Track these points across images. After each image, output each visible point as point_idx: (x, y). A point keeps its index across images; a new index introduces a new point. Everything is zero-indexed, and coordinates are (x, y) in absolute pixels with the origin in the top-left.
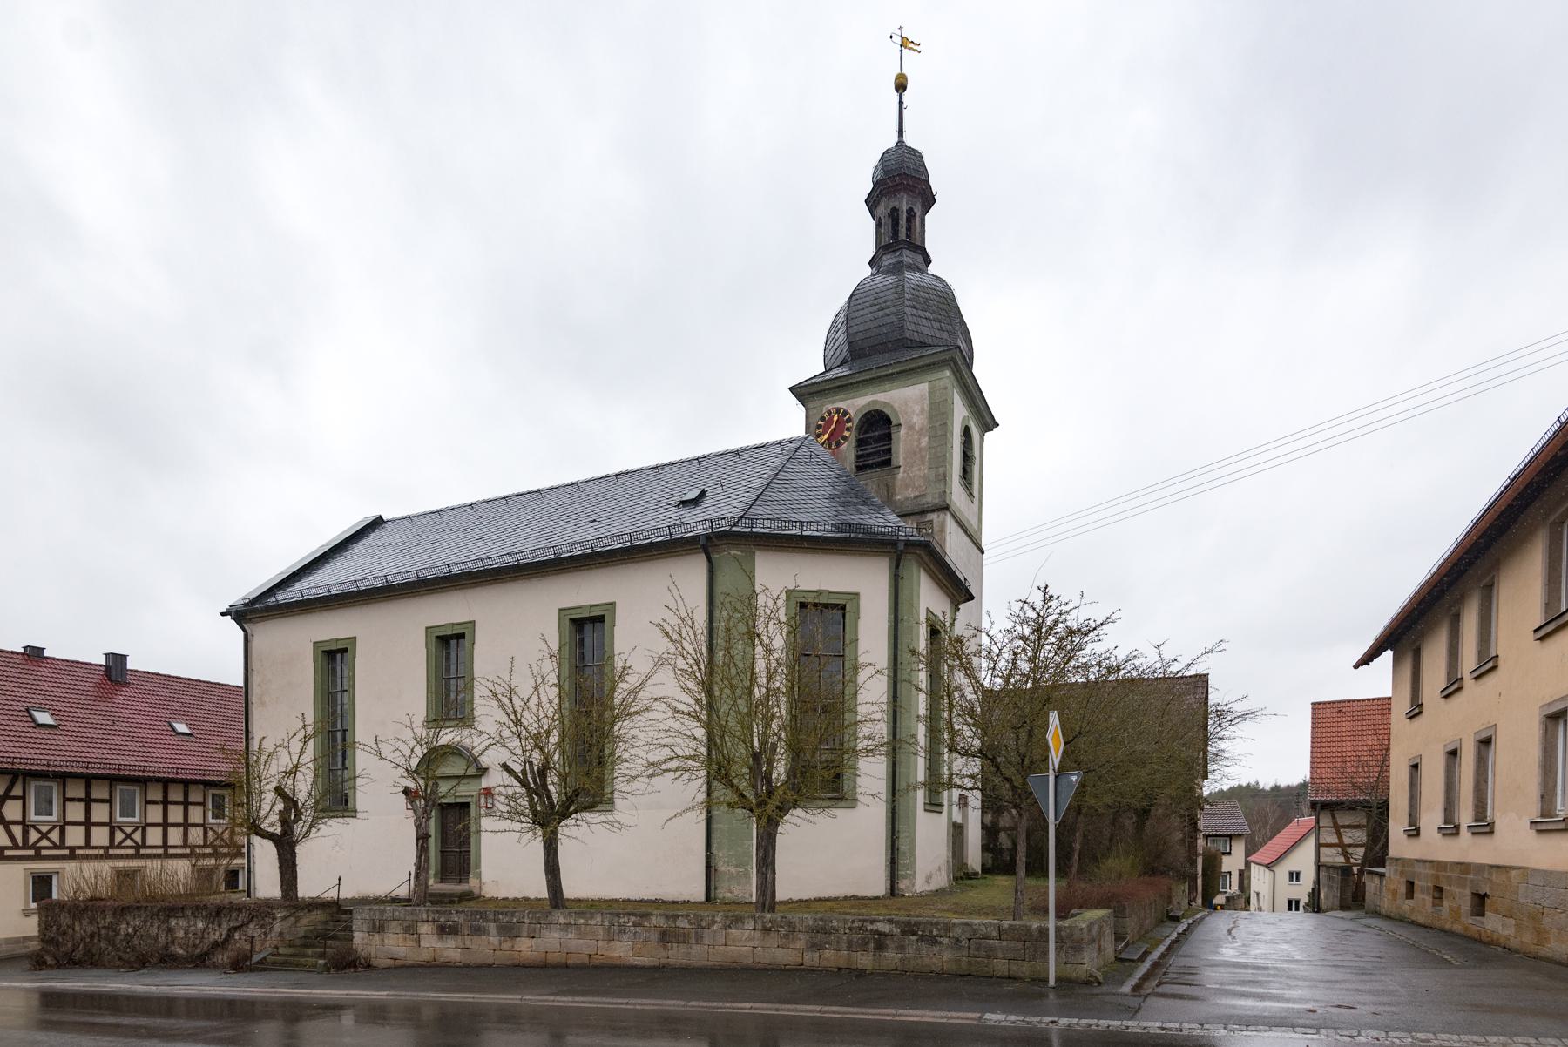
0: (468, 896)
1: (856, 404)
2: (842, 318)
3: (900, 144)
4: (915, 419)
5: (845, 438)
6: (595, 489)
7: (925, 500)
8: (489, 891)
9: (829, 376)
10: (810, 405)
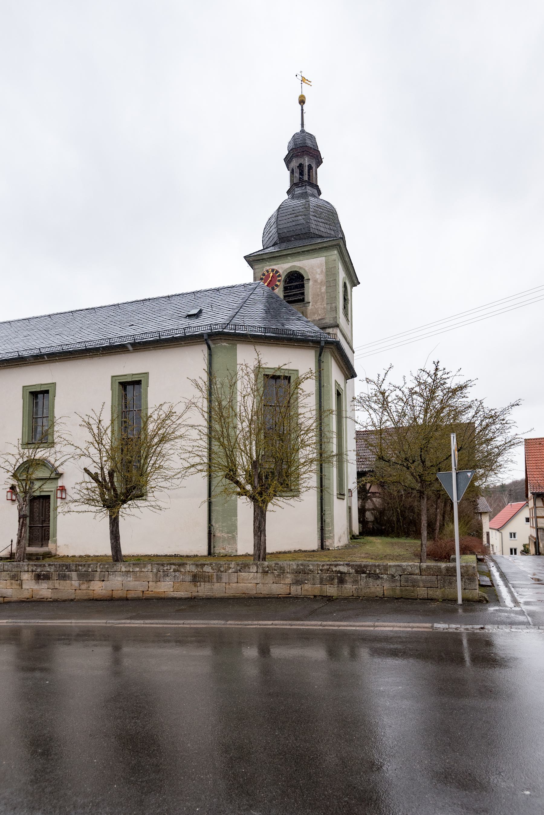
0: (48, 555)
1: (284, 267)
2: (273, 220)
3: (303, 131)
4: (318, 276)
5: (277, 286)
6: (130, 308)
7: (324, 322)
8: (62, 551)
9: (267, 251)
10: (256, 267)
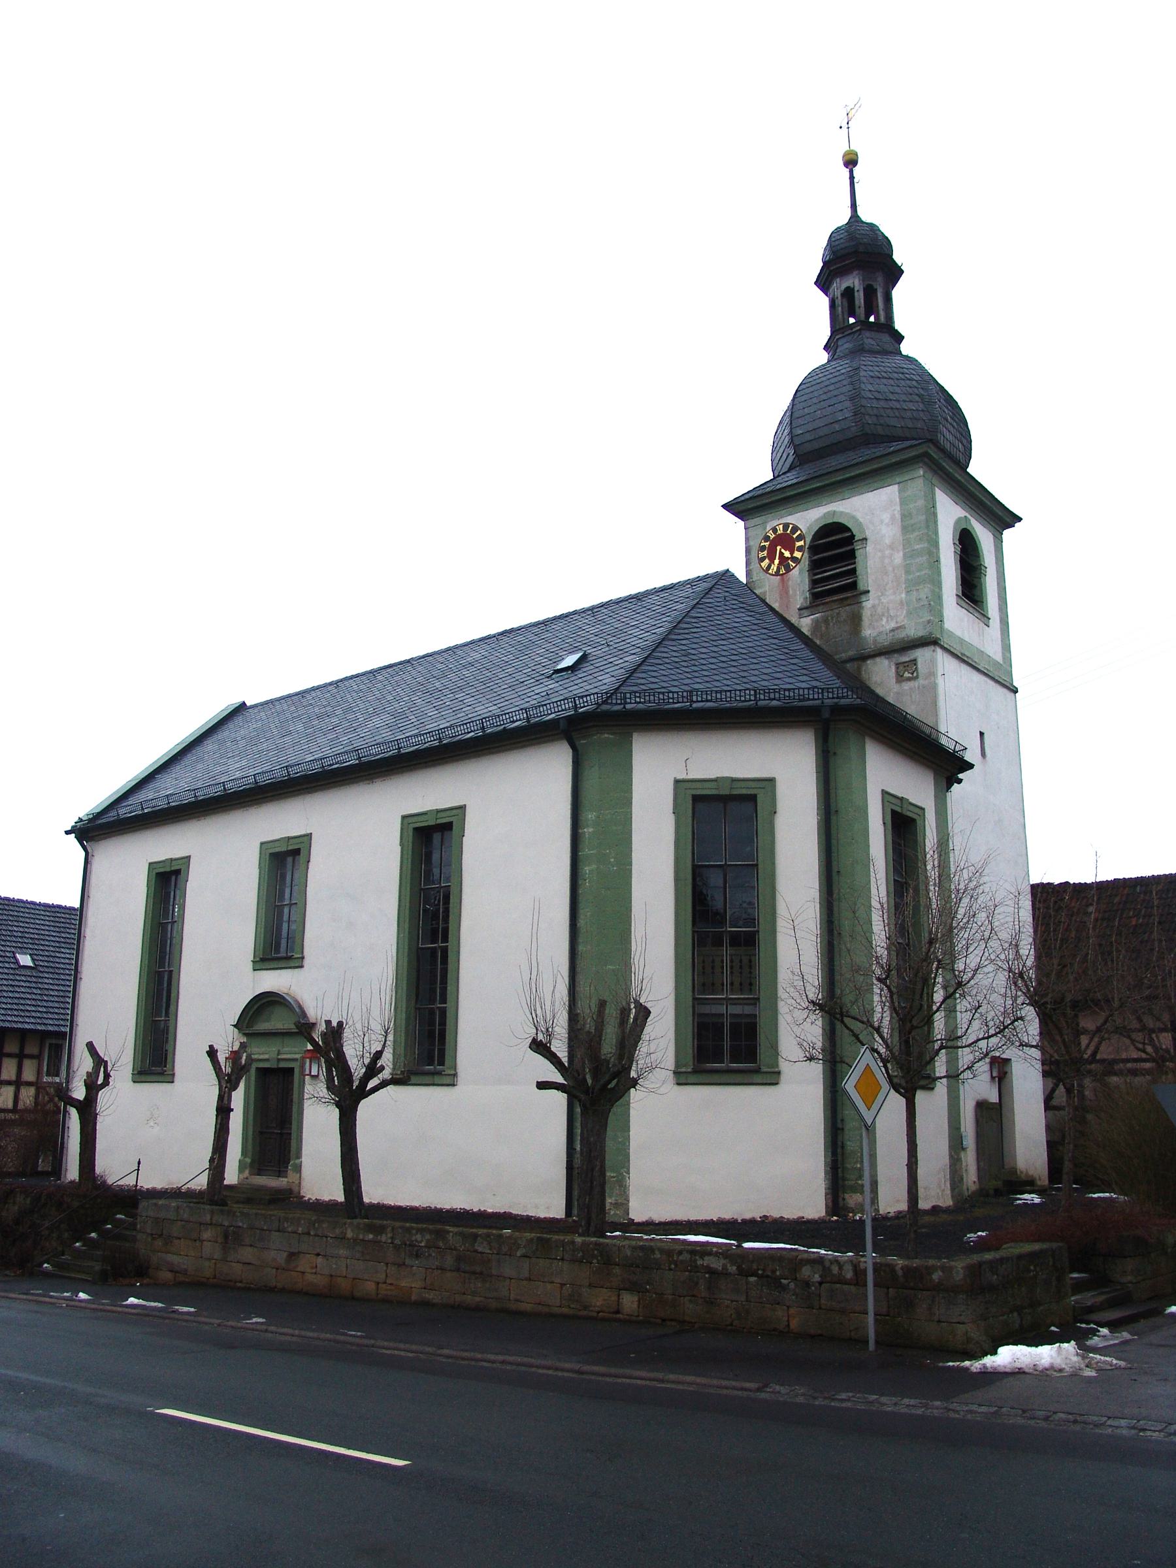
1: (807, 519)
5: (786, 526)
